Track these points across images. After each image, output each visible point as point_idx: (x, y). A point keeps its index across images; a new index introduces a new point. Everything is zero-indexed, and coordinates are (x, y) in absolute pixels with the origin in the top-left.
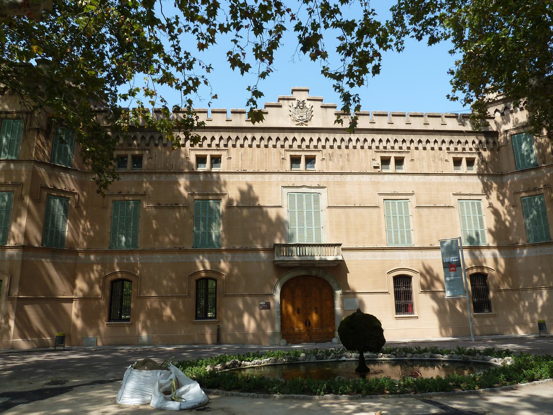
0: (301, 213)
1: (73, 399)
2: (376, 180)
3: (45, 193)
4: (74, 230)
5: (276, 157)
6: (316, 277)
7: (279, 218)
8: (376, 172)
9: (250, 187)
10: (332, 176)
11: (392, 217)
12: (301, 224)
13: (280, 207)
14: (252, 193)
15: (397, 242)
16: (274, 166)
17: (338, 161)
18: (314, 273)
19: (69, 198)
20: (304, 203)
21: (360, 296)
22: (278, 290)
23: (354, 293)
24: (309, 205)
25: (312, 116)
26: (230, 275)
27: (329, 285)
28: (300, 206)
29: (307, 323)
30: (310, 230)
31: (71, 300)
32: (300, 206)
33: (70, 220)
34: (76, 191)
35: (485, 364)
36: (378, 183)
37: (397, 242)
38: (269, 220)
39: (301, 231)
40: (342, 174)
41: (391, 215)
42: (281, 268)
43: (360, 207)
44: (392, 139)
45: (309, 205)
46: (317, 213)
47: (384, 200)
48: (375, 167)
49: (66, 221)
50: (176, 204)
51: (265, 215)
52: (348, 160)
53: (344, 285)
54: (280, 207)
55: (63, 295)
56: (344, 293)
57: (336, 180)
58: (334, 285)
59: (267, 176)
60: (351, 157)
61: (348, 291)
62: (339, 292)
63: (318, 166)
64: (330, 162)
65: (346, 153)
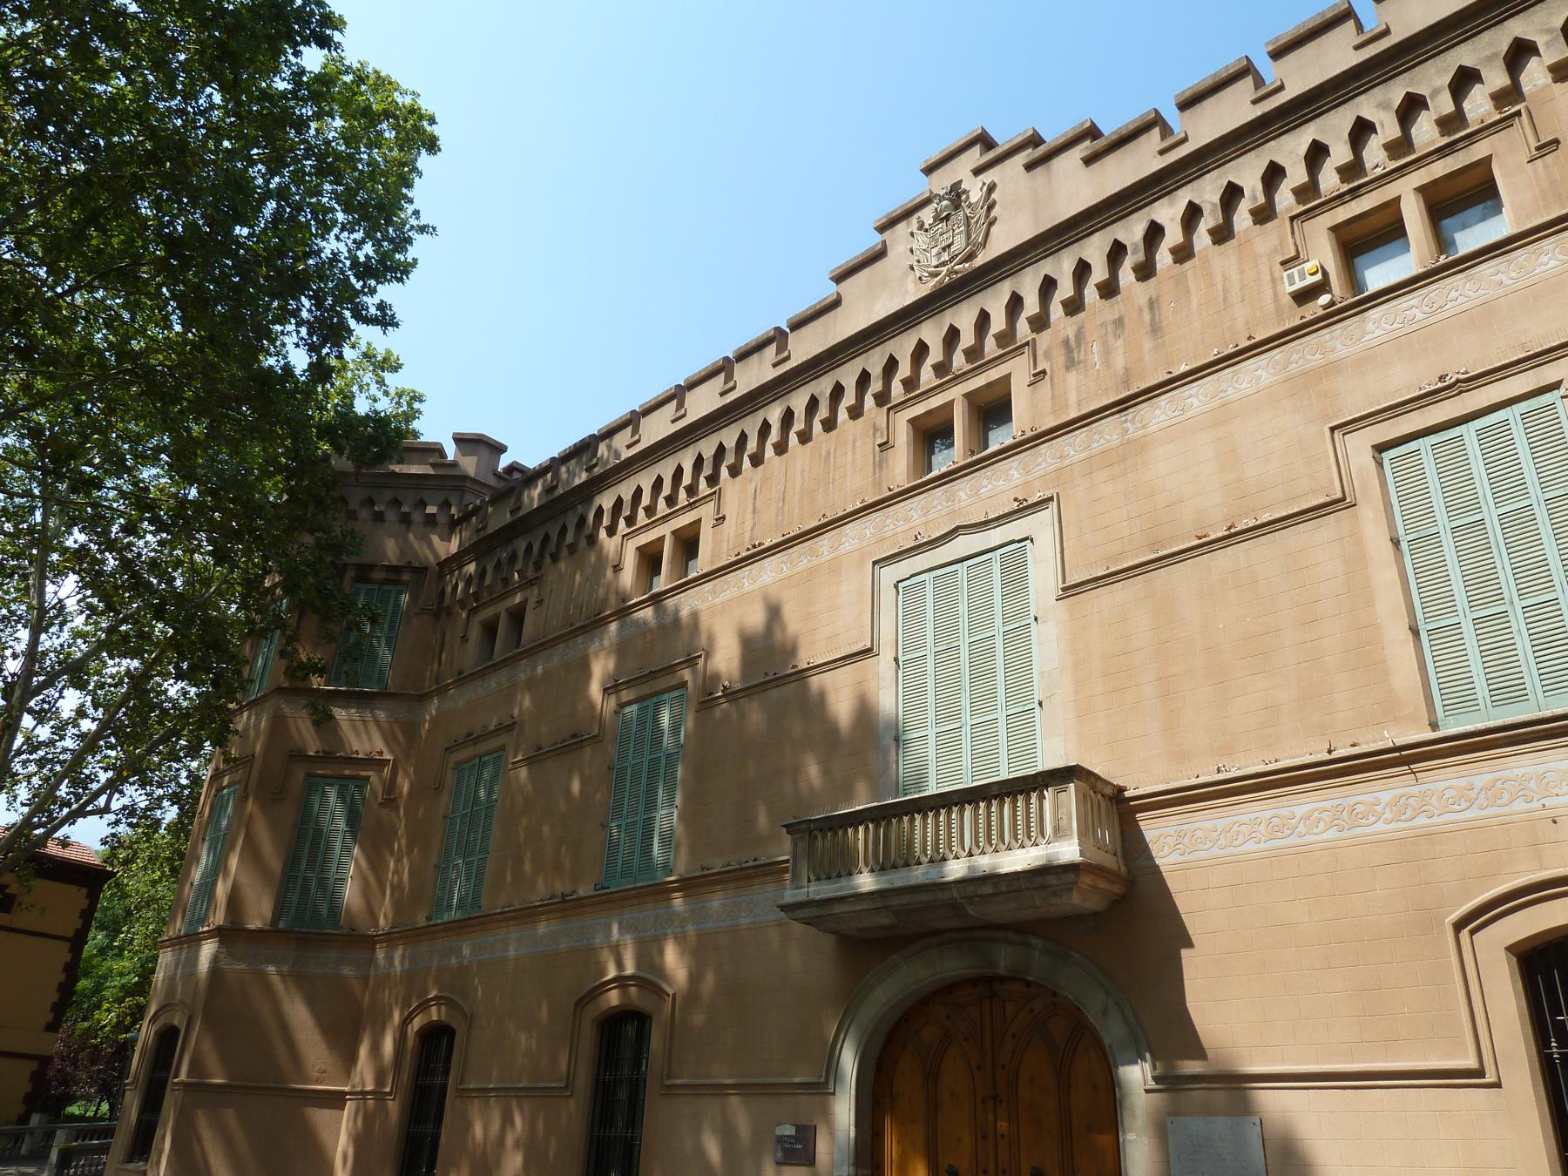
2: (1317, 360)
3: (300, 774)
4: (372, 880)
5: (858, 451)
7: (865, 712)
8: (1323, 308)
9: (774, 612)
10: (1081, 435)
11: (1447, 541)
12: (947, 713)
14: (778, 636)
15: (1506, 691)
16: (855, 487)
17: (1107, 353)
18: (1004, 959)
19: (367, 779)
20: (963, 608)
21: (1273, 1102)
23: (1235, 1086)
24: (980, 611)
25: (991, 224)
26: (693, 994)
30: (983, 730)
31: (335, 1100)
33: (363, 848)
34: (387, 756)
35: (282, 1089)
36: (1332, 369)
37: (1506, 691)
38: (830, 729)
39: (948, 741)
40: (1122, 405)
41: (1443, 523)
43: (1232, 537)
44: (1384, 106)
47: (1381, 448)
48: (1303, 296)
49: (350, 850)
50: (574, 736)
51: (816, 706)
52: (1155, 329)
53: (1171, 1035)
55: (318, 1082)
56: (1168, 1082)
57: (1097, 446)
58: (1112, 1031)
59: (824, 543)
60: (1167, 309)
61: (1192, 1067)
62: (1137, 1075)
63: (1026, 412)
64: (1072, 378)
65: (1143, 300)
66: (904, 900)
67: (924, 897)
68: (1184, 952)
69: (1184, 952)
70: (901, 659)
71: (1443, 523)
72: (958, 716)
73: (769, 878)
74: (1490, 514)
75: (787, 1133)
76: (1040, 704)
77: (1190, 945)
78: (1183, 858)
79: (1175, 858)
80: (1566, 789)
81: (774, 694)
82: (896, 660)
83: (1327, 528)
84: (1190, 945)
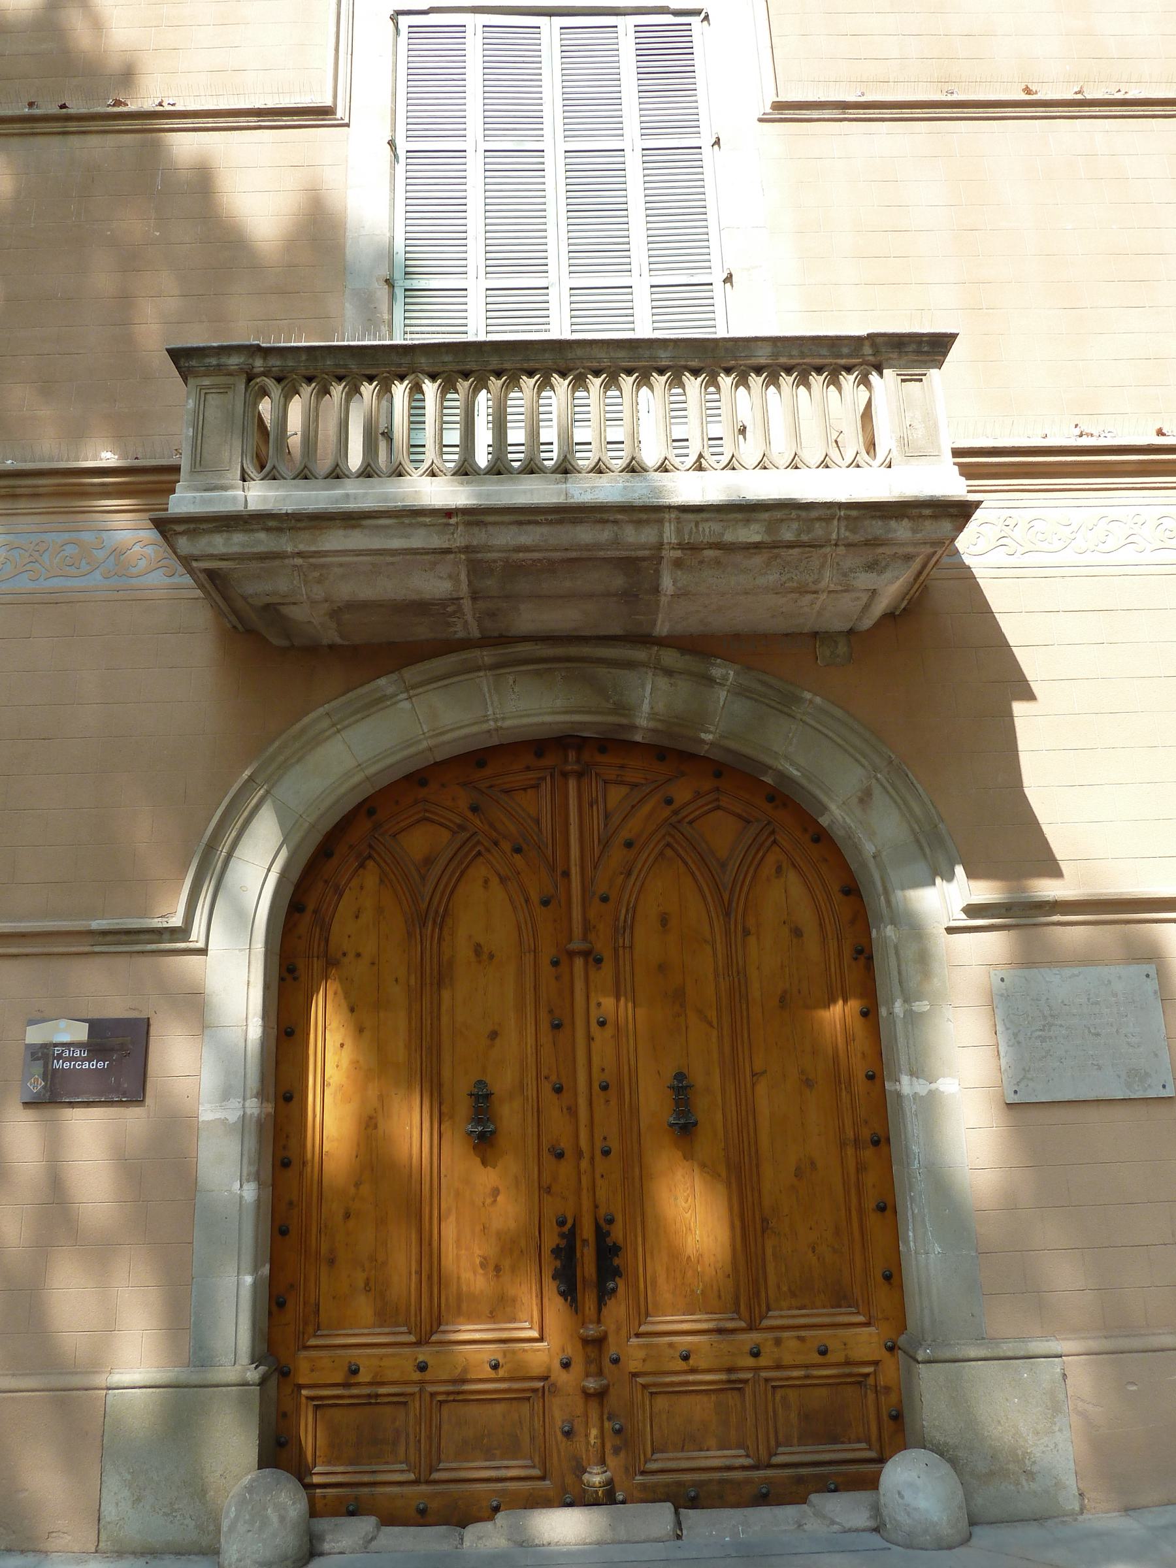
0: (515, 167)
1: (312, 1185)
6: (672, 754)
13: (321, 114)
18: (650, 700)
22: (258, 869)
27: (821, 837)
28: (513, 112)
29: (590, 1260)
32: (513, 112)
38: (220, 248)
41: (474, 140)
42: (285, 630)
45: (590, 105)
46: (678, 162)
54: (321, 114)
58: (875, 831)
62: (943, 901)
66: (529, 536)
67: (585, 534)
68: (1019, 708)
69: (1019, 708)
70: (402, 146)
71: (474, 140)
72: (542, 268)
73: (23, 504)
74: (554, 144)
75: (65, 1038)
76: (729, 279)
77: (1030, 696)
78: (1013, 561)
79: (998, 557)
80: (1168, 1340)
81: (53, 149)
82: (392, 143)
83: (785, 97)
84: (1030, 696)
